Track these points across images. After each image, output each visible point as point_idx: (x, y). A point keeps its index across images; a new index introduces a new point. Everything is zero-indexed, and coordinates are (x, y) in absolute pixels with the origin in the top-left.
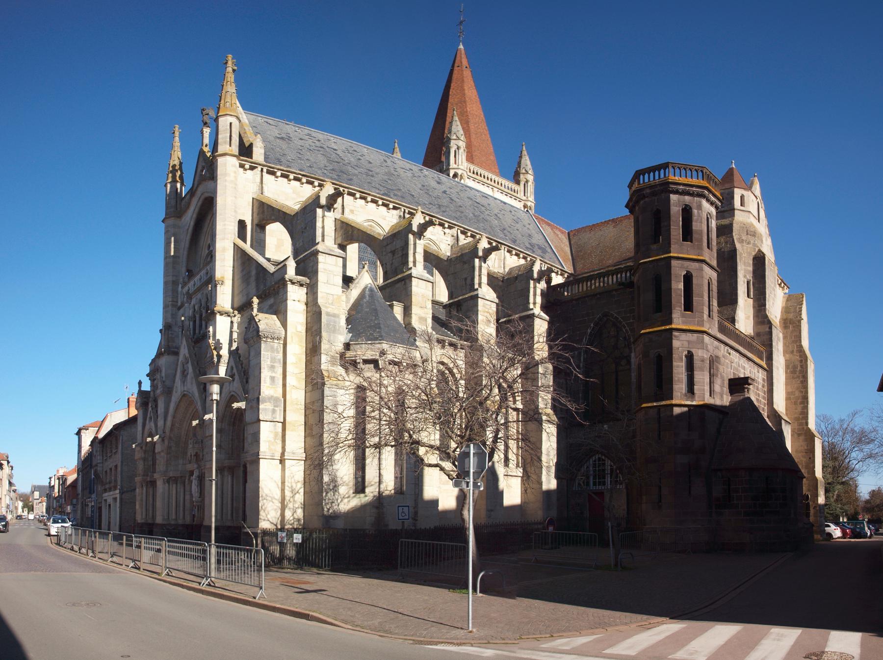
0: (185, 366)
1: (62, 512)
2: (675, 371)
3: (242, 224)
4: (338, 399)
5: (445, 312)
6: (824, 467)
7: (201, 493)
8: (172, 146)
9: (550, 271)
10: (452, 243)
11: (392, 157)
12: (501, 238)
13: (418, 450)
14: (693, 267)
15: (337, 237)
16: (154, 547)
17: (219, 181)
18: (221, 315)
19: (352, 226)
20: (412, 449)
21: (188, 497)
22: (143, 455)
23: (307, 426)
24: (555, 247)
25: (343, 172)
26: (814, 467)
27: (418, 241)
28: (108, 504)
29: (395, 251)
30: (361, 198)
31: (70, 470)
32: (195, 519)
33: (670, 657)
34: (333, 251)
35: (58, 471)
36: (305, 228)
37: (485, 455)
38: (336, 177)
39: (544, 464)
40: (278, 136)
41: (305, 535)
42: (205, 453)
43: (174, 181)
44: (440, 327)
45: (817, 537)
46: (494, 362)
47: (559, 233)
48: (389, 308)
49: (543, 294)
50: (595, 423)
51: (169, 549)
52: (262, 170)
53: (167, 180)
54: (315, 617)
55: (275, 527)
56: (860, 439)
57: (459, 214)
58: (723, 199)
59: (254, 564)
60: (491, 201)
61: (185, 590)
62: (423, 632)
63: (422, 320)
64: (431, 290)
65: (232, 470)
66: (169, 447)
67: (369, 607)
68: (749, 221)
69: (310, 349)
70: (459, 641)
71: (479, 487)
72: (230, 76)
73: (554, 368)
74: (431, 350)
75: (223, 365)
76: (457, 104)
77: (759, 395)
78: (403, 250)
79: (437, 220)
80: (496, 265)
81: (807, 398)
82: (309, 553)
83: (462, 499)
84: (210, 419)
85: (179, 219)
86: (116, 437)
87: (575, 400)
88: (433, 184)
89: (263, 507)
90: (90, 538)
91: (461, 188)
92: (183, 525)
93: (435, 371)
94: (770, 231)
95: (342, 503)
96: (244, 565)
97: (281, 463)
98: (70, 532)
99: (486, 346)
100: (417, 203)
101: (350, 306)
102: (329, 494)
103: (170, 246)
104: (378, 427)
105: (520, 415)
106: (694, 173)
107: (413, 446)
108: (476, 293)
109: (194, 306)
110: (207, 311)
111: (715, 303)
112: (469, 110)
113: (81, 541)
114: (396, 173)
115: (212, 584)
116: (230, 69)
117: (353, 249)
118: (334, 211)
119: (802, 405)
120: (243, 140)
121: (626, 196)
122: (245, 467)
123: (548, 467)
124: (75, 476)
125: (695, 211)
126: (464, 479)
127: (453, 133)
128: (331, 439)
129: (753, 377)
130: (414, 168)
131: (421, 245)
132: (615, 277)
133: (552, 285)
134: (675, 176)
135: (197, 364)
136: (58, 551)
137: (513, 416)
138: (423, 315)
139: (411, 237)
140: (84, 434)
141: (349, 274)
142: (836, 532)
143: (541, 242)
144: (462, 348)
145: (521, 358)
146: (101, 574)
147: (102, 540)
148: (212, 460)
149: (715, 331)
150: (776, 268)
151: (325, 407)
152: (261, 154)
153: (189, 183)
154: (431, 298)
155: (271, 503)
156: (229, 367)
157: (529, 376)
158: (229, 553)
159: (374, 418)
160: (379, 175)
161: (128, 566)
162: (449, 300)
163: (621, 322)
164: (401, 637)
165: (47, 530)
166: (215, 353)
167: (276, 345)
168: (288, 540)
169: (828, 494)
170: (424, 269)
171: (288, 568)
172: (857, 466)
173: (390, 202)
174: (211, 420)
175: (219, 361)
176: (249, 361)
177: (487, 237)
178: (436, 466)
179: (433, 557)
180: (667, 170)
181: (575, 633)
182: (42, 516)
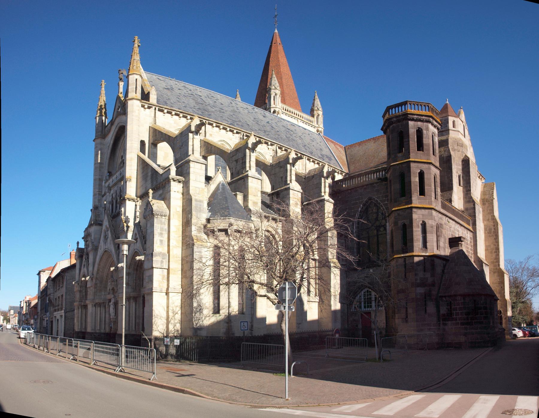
0: (106, 233)
1: (28, 324)
2: (414, 234)
3: (142, 143)
4: (202, 254)
5: (269, 199)
6: (510, 292)
7: (115, 314)
8: (100, 94)
9: (334, 171)
10: (273, 155)
11: (235, 101)
12: (303, 151)
13: (253, 286)
14: (424, 167)
15: (201, 151)
16: (86, 347)
17: (129, 116)
18: (129, 200)
19: (211, 145)
20: (249, 285)
21: (107, 316)
22: (79, 289)
23: (183, 271)
24: (337, 157)
25: (205, 110)
26: (504, 293)
27: (252, 154)
28: (57, 319)
29: (238, 159)
30: (216, 126)
31: (33, 297)
32: (112, 330)
33: (415, 416)
34: (199, 160)
35: (26, 297)
36: (182, 146)
37: (296, 289)
38: (201, 113)
39: (332, 293)
40: (165, 87)
41: (182, 340)
42: (118, 288)
43: (101, 115)
44: (266, 209)
45: (507, 337)
46: (300, 230)
47: (339, 147)
48: (234, 197)
49: (330, 186)
50: (364, 268)
51: (95, 348)
52: (155, 109)
53: (97, 114)
54: (188, 391)
55: (163, 335)
56: (533, 274)
57: (277, 136)
58: (442, 123)
59: (149, 358)
60: (297, 128)
61: (105, 374)
62: (257, 400)
63: (255, 203)
64: (261, 184)
65: (135, 299)
66: (96, 284)
67: (223, 385)
69: (185, 223)
70: (280, 406)
71: (292, 309)
72: (136, 50)
73: (338, 233)
74: (261, 222)
75: (130, 232)
77: (468, 248)
78: (243, 159)
79: (264, 140)
80: (301, 168)
81: (499, 249)
82: (184, 352)
83: (281, 316)
84: (122, 266)
85: (103, 139)
86: (63, 277)
87: (352, 254)
88: (261, 117)
89: (155, 323)
90: (45, 340)
91: (278, 120)
92: (104, 334)
93: (263, 236)
94: (472, 143)
95: (205, 320)
96: (143, 359)
97: (166, 295)
98: (33, 336)
99: (295, 220)
100: (251, 129)
101: (210, 195)
102: (197, 315)
103: (98, 156)
104: (228, 272)
105: (317, 263)
106: (423, 107)
107: (250, 284)
108: (288, 186)
109: (112, 195)
110: (120, 198)
111: (439, 190)
112: (282, 71)
113: (40, 342)
114: (238, 111)
115: (123, 371)
116: (136, 45)
117: (212, 159)
118: (200, 135)
119: (496, 254)
120: (144, 90)
121: (381, 122)
122: (144, 297)
123: (335, 296)
124: (36, 301)
125: (425, 132)
126: (282, 304)
127: (272, 85)
128: (198, 279)
129: (464, 236)
130: (249, 107)
131: (254, 156)
132: (375, 174)
133: (335, 180)
134: (411, 109)
135: (114, 231)
136: (25, 348)
137: (312, 264)
138: (256, 201)
139: (247, 151)
140: (42, 274)
141: (209, 175)
142: (519, 333)
143: (328, 153)
144: (280, 222)
145: (318, 227)
146: (52, 363)
147: (53, 342)
148: (123, 293)
149: (439, 208)
150: (477, 166)
151: (194, 259)
152: (155, 98)
153: (110, 117)
154: (260, 190)
155: (160, 320)
156: (134, 234)
157: (322, 238)
158: (134, 351)
159: (225, 266)
160: (228, 112)
161: (70, 358)
162: (272, 191)
163: (380, 204)
164: (243, 404)
165: (18, 334)
166: (125, 225)
167: (163, 220)
168: (171, 343)
169: (513, 310)
170: (256, 172)
171: (171, 361)
172: (531, 291)
173: (235, 129)
174: (122, 267)
175: (127, 230)
176: (147, 230)
177: (295, 151)
178: (265, 296)
179: (263, 353)
180: (406, 106)
181: (354, 402)
182: (15, 326)
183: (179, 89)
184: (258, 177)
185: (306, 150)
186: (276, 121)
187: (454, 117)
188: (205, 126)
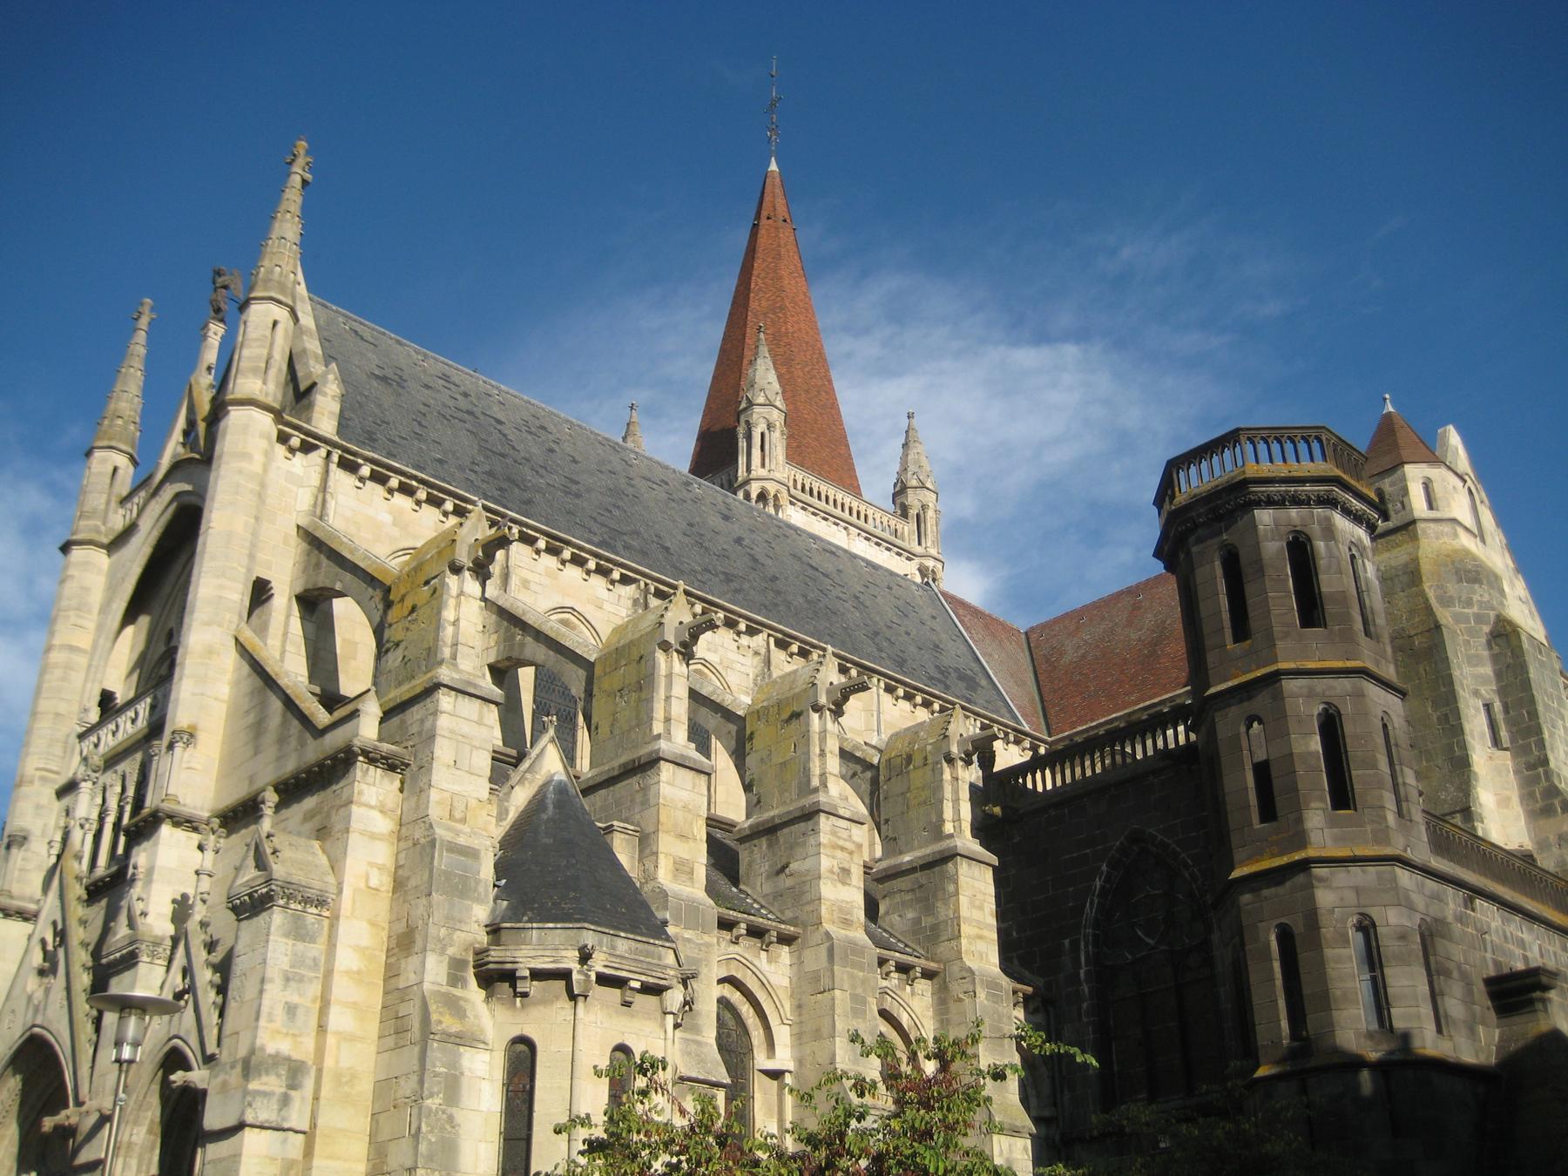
34: (475, 686)
38: (496, 493)
52: (329, 454)
57: (771, 595)
64: (706, 793)
68: (1456, 544)
76: (765, 314)
88: (715, 521)
114: (630, 490)
121: (1150, 528)
125: (1320, 546)
133: (995, 770)
149: (1422, 852)
183: (427, 387)
184: (695, 760)
185: (880, 650)
186: (766, 536)
187: (1424, 465)
188: (508, 551)
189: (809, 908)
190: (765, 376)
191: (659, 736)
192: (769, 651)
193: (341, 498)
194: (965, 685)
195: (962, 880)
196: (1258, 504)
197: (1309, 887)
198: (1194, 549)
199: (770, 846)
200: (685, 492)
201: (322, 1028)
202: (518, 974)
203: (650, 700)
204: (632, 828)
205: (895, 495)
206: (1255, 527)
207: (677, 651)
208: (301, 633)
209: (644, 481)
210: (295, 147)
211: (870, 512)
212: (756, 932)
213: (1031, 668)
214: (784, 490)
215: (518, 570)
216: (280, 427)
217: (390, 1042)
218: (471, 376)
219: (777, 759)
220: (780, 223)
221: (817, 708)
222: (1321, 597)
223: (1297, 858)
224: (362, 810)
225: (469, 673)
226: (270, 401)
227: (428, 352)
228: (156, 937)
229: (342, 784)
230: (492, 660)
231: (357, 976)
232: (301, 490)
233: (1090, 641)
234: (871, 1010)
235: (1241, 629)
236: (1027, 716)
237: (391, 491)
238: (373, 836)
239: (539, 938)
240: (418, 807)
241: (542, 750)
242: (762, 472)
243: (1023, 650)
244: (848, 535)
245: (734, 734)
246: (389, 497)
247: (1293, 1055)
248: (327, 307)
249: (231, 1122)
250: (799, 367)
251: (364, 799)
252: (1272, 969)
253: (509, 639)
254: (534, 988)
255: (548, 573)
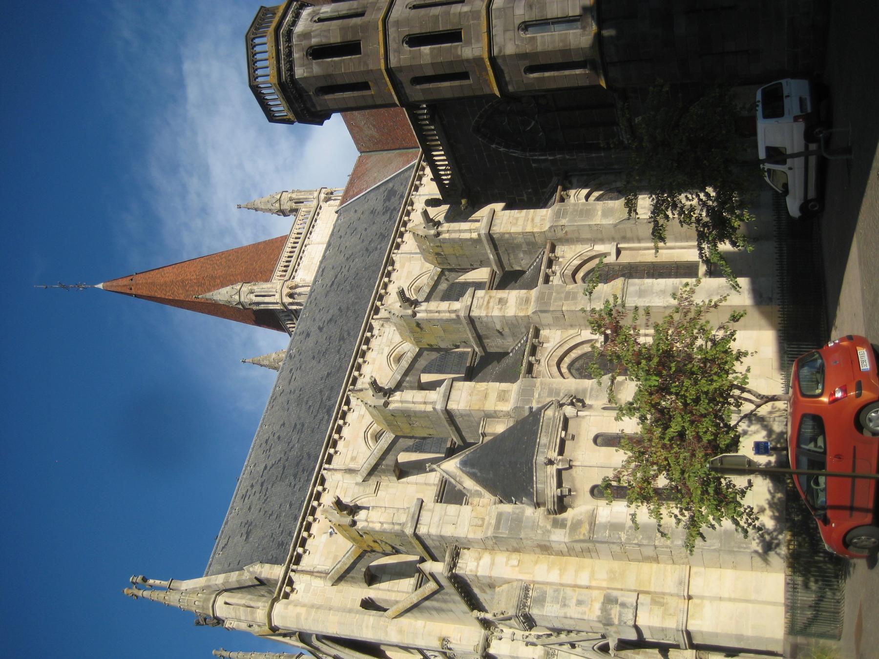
34: (414, 514)
38: (306, 474)
52: (293, 571)
57: (350, 314)
88: (310, 342)
100: (338, 370)
125: (314, 41)
133: (441, 198)
183: (250, 509)
185: (376, 249)
186: (317, 311)
189: (520, 321)
190: (223, 294)
191: (434, 408)
192: (381, 318)
193: (316, 562)
194: (393, 197)
195: (502, 230)
196: (292, 76)
197: (504, 57)
198: (319, 108)
199: (488, 338)
200: (295, 359)
201: (587, 587)
202: (559, 495)
203: (415, 412)
204: (482, 422)
205: (285, 215)
206: (305, 78)
207: (388, 398)
208: (388, 583)
209: (292, 383)
210: (128, 594)
211: (296, 231)
212: (534, 351)
213: (381, 152)
214: (287, 284)
215: (347, 463)
216: (281, 598)
217: (594, 554)
218: (241, 481)
219: (442, 333)
220: (133, 282)
221: (414, 314)
222: (344, 42)
223: (489, 63)
224: (480, 569)
225: (408, 516)
226: (268, 605)
227: (230, 506)
228: (544, 654)
229: (467, 579)
230: (395, 479)
231: (562, 570)
232: (313, 585)
233: (365, 122)
234: (572, 289)
235: (365, 86)
236: (408, 161)
237: (310, 535)
238: (493, 564)
239: (541, 483)
240: (477, 543)
241: (444, 471)
242: (277, 296)
243: (371, 156)
244: (309, 244)
245: (429, 352)
246: (313, 536)
247: (594, 67)
248: (211, 564)
249: (634, 631)
250: (216, 273)
251: (474, 569)
252: (548, 77)
253: (384, 472)
254: (566, 485)
255: (347, 446)
